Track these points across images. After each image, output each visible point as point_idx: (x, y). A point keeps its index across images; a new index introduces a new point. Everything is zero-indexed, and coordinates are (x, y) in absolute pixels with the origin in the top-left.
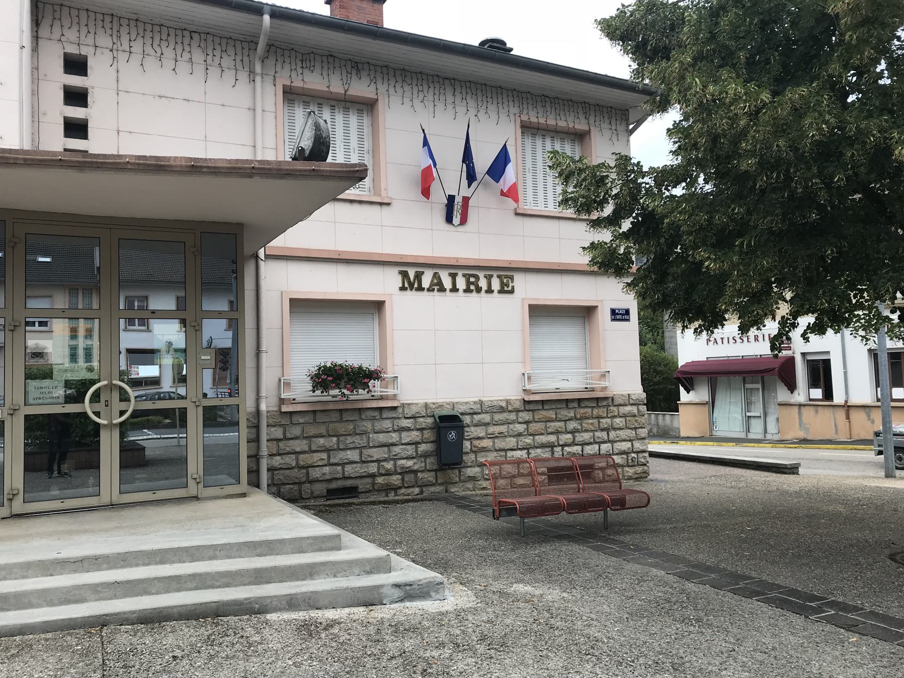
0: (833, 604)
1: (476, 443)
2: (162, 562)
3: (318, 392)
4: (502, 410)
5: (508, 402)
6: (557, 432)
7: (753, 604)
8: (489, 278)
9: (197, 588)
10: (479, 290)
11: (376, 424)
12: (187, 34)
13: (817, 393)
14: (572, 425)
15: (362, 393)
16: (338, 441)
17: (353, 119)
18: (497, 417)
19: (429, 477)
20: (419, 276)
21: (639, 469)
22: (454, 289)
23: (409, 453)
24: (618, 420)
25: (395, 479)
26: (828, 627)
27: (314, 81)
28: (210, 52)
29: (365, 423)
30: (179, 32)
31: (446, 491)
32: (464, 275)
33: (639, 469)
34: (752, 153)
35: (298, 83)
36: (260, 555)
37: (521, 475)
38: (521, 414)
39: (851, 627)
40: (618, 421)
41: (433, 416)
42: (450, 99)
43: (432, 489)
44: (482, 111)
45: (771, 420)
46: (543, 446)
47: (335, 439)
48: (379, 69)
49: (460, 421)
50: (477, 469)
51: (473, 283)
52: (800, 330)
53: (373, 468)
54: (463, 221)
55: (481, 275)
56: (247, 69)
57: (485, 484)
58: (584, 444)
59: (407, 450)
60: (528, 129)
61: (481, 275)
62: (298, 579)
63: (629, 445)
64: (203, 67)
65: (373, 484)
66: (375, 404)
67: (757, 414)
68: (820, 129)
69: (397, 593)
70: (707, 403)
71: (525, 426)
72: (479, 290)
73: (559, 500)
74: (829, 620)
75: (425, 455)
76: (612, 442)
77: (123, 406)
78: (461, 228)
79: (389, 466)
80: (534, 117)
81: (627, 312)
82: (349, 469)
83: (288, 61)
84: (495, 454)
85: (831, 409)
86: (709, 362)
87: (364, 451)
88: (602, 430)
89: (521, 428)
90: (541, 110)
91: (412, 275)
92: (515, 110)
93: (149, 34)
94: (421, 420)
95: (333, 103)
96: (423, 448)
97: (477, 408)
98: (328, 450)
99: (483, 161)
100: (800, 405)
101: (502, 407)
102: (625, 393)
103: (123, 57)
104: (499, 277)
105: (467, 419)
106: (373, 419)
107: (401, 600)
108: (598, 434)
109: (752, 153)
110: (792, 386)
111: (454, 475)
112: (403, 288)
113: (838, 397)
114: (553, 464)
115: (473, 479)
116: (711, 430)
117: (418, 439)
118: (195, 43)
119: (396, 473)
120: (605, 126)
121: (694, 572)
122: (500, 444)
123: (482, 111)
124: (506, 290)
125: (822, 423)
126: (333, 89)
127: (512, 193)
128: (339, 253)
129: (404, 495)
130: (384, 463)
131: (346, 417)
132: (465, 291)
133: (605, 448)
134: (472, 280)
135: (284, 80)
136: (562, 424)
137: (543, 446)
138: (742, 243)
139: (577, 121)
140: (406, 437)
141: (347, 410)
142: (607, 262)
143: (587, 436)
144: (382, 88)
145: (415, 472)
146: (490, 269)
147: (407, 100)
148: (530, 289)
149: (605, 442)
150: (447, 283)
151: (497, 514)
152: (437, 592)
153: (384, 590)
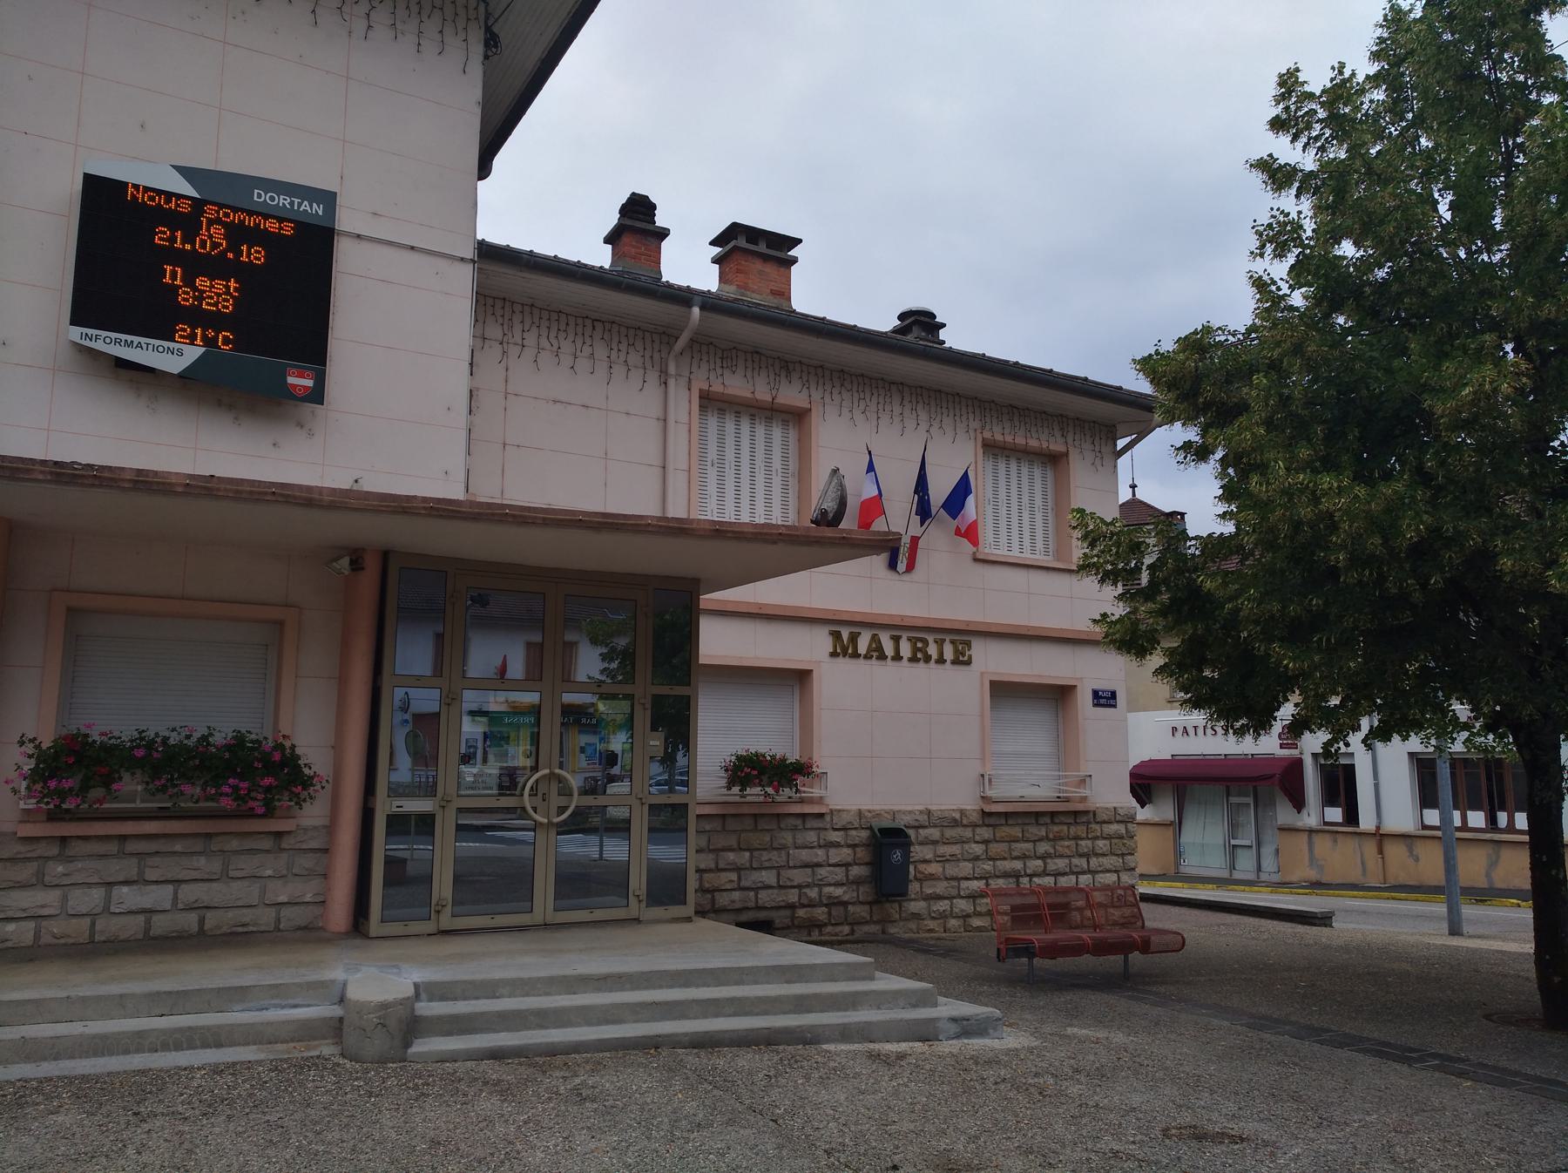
0: (1435, 1056)
1: (922, 867)
2: (687, 985)
3: (736, 790)
4: (955, 823)
5: (962, 812)
6: (1023, 857)
7: (1344, 1053)
8: (940, 643)
9: (735, 1015)
10: (927, 659)
11: (799, 835)
12: (588, 322)
13: (1335, 814)
14: (1043, 848)
15: (787, 792)
16: (752, 857)
17: (777, 433)
18: (949, 833)
19: (862, 911)
20: (854, 638)
21: (1127, 911)
22: (897, 657)
23: (838, 878)
24: (1101, 843)
25: (820, 913)
26: (1437, 1075)
27: (736, 384)
28: (614, 346)
29: (784, 834)
30: (580, 321)
31: (883, 932)
32: (909, 639)
33: (1127, 911)
34: (1343, 547)
35: (717, 388)
36: (788, 982)
37: (979, 914)
38: (978, 830)
39: (1462, 1074)
40: (1102, 844)
41: (871, 828)
42: (897, 410)
43: (866, 928)
44: (936, 425)
45: (1268, 851)
46: (1006, 875)
47: (747, 854)
48: (812, 370)
49: (907, 836)
50: (923, 904)
51: (920, 650)
52: (1361, 735)
53: (793, 896)
54: (910, 567)
55: (931, 639)
56: (657, 367)
57: (932, 924)
58: (1058, 874)
59: (835, 872)
60: (992, 449)
61: (931, 639)
62: (839, 1010)
63: (1114, 877)
64: (605, 365)
65: (793, 918)
66: (797, 809)
67: (1247, 843)
68: (1418, 529)
69: (954, 1028)
70: (1171, 824)
71: (983, 847)
72: (927, 659)
73: (1065, 938)
74: (1436, 1068)
75: (857, 882)
76: (1094, 872)
77: (562, 801)
78: (906, 577)
79: (813, 893)
80: (1000, 433)
81: (1113, 695)
82: (764, 896)
83: (705, 358)
84: (945, 883)
85: (1357, 839)
86: (1175, 761)
87: (783, 872)
88: (1081, 856)
89: (978, 849)
90: (1007, 425)
91: (845, 636)
92: (975, 424)
93: (545, 323)
94: (854, 833)
95: (753, 411)
96: (856, 871)
97: (923, 819)
98: (738, 869)
99: (939, 491)
100: (1311, 831)
101: (955, 820)
102: (1110, 806)
103: (514, 351)
104: (952, 642)
105: (911, 832)
106: (795, 829)
107: (958, 1037)
108: (1075, 861)
109: (1343, 547)
110: (1299, 803)
111: (892, 909)
112: (834, 654)
113: (1367, 822)
114: (1018, 901)
115: (916, 916)
116: (1177, 864)
117: (850, 859)
118: (598, 333)
119: (821, 904)
120: (1087, 446)
121: (1261, 1023)
122: (951, 870)
123: (936, 425)
124: (961, 660)
125: (1341, 858)
126: (759, 396)
127: (970, 533)
128: (761, 606)
129: (830, 934)
130: (807, 890)
131: (762, 825)
132: (910, 660)
133: (1085, 880)
134: (919, 645)
135: (699, 384)
136: (1029, 846)
137: (1006, 875)
138: (1320, 639)
139: (1052, 439)
140: (836, 856)
141: (763, 815)
142: (1129, 639)
143: (1061, 864)
144: (817, 395)
145: (845, 904)
146: (942, 631)
147: (845, 411)
148: (993, 661)
149: (1084, 873)
150: (889, 649)
151: (1003, 954)
152: (995, 1029)
153: (940, 1024)
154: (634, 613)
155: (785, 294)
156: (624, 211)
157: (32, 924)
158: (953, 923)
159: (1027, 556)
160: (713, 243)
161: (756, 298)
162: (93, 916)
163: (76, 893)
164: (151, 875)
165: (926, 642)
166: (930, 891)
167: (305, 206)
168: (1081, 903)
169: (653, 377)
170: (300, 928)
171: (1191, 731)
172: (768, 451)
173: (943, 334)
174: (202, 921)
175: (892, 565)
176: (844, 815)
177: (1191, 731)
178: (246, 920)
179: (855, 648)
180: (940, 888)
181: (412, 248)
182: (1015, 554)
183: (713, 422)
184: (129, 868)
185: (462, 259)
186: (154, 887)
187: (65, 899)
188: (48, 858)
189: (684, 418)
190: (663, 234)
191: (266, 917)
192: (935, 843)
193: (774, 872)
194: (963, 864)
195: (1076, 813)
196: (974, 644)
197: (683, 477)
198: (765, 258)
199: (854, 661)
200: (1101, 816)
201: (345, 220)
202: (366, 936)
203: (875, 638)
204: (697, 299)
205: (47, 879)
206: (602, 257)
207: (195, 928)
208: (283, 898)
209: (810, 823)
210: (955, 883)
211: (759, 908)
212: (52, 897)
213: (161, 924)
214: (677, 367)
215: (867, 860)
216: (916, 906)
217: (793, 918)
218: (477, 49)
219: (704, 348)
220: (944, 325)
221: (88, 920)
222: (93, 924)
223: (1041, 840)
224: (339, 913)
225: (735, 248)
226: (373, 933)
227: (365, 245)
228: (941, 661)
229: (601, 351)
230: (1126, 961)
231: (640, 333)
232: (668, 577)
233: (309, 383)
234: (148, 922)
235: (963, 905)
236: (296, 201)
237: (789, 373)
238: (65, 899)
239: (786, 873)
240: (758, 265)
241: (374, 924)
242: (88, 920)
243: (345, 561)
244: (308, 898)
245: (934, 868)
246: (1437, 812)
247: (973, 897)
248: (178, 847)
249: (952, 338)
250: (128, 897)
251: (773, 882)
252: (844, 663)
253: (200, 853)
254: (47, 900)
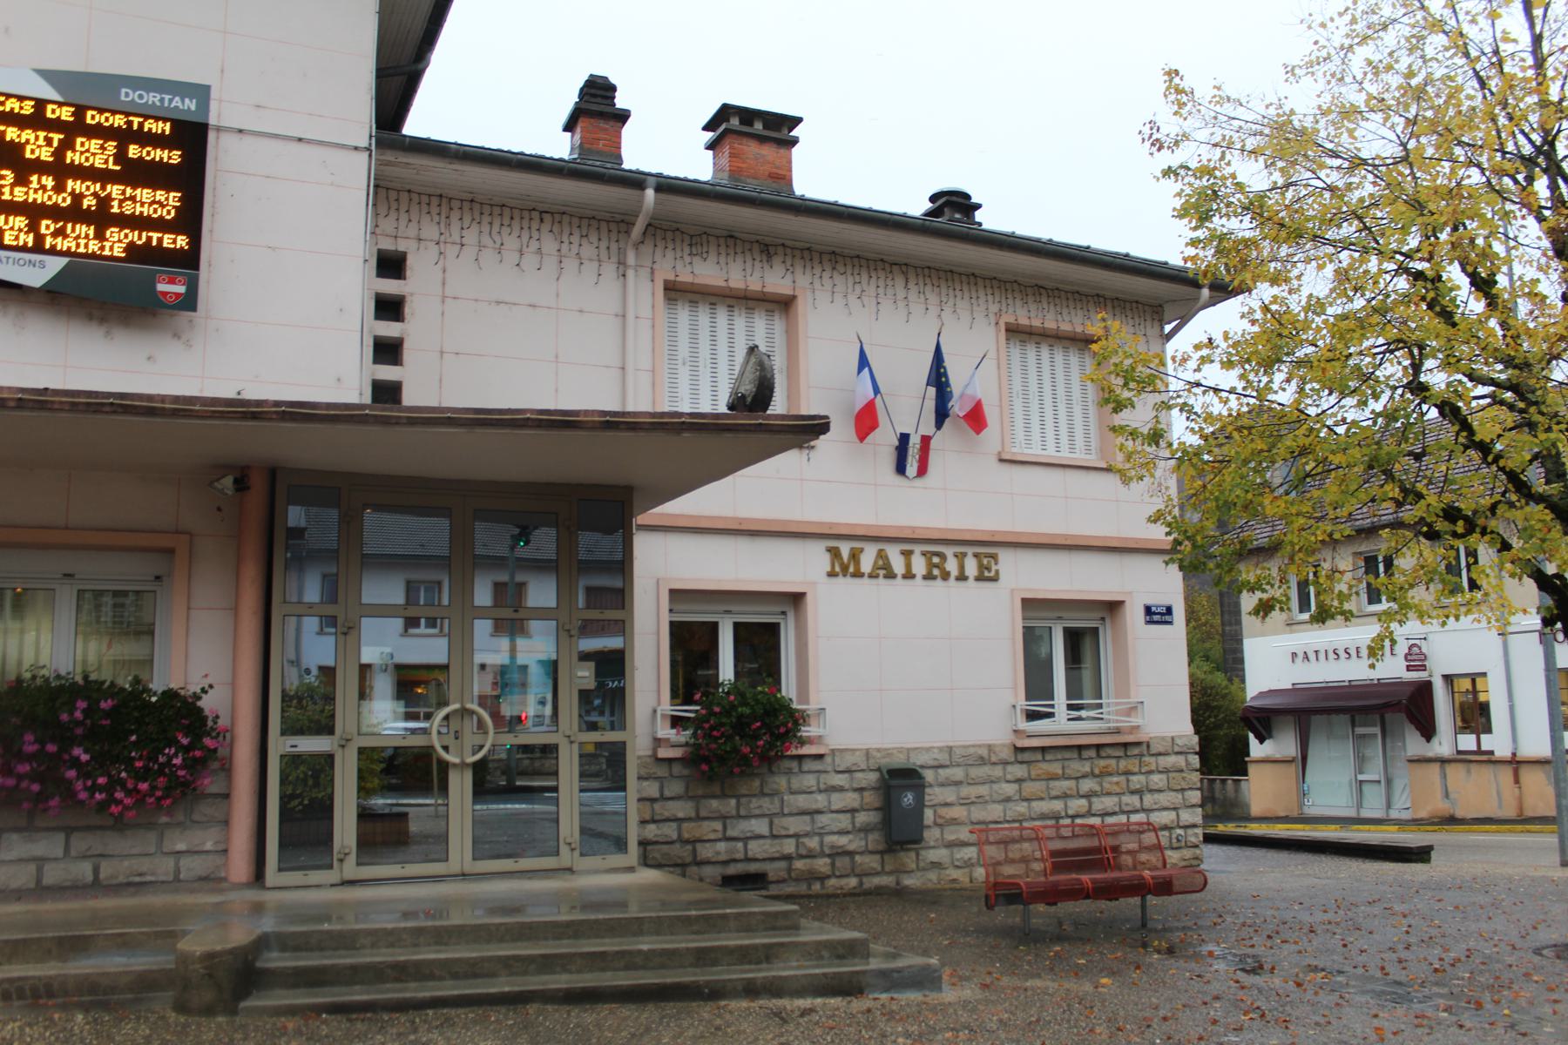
1: (943, 811)
4: (982, 761)
5: (990, 747)
8: (960, 557)
10: (946, 576)
12: (536, 215)
14: (1087, 785)
18: (977, 772)
19: (872, 862)
20: (855, 556)
21: (1188, 853)
24: (1155, 778)
25: (822, 865)
27: (708, 271)
28: (565, 238)
30: (526, 214)
35: (685, 277)
37: (1013, 861)
38: (1009, 768)
40: (1158, 780)
42: (901, 293)
44: (948, 310)
48: (798, 253)
49: (920, 777)
51: (936, 566)
53: (789, 847)
54: (922, 471)
56: (614, 259)
61: (949, 551)
63: (1173, 815)
64: (555, 260)
65: (789, 870)
67: (1375, 777)
71: (1015, 786)
72: (946, 576)
75: (865, 830)
76: (1148, 811)
78: (919, 482)
79: (813, 843)
81: (1169, 610)
82: (755, 848)
83: (671, 246)
85: (1491, 767)
87: (776, 821)
88: (1132, 793)
89: (1010, 789)
91: (845, 554)
93: (486, 219)
95: (731, 301)
96: (862, 818)
97: (943, 758)
98: (724, 818)
100: (1443, 761)
101: (982, 758)
104: (976, 555)
108: (1126, 799)
111: (909, 859)
112: (832, 574)
114: (1058, 845)
115: (936, 865)
116: (1301, 805)
117: (856, 805)
119: (823, 854)
124: (986, 576)
126: (733, 284)
128: (741, 520)
130: (805, 840)
132: (925, 578)
134: (936, 560)
136: (1072, 783)
137: (1043, 817)
140: (838, 800)
145: (851, 854)
147: (838, 298)
149: (1136, 811)
150: (898, 565)
159: (1065, 455)
160: (706, 128)
166: (952, 837)
167: (177, 102)
169: (610, 269)
171: (1312, 656)
173: (979, 216)
174: (96, 871)
175: (901, 469)
177: (1312, 656)
181: (300, 140)
182: (1050, 454)
183: (683, 314)
185: (356, 148)
189: (646, 312)
190: (623, 117)
192: (958, 783)
193: (766, 820)
194: (991, 807)
195: (1125, 745)
196: (1001, 557)
197: (645, 379)
199: (857, 581)
201: (216, 116)
203: (881, 554)
204: (652, 180)
206: (560, 146)
211: (748, 860)
214: (637, 256)
215: (877, 805)
216: (933, 855)
217: (789, 870)
219: (669, 234)
220: (978, 206)
223: (1084, 776)
225: (726, 131)
227: (248, 139)
228: (962, 577)
229: (550, 245)
230: (1143, 906)
231: (594, 223)
232: (548, 484)
233: (181, 289)
236: (167, 97)
237: (769, 257)
243: (228, 481)
245: (958, 812)
246: (553, 604)
249: (988, 219)
251: (765, 830)
252: (842, 582)
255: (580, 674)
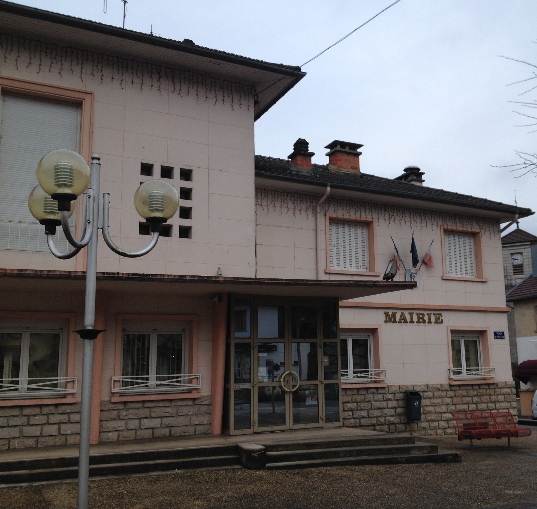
1: (426, 408)
4: (439, 390)
5: (441, 385)
6: (468, 403)
10: (424, 322)
14: (476, 399)
18: (437, 394)
19: (401, 427)
20: (394, 315)
22: (412, 322)
24: (500, 397)
38: (448, 392)
40: (501, 398)
47: (355, 404)
49: (420, 395)
57: (431, 432)
61: (425, 313)
71: (451, 399)
72: (424, 322)
75: (400, 415)
80: (450, 226)
84: (436, 415)
87: (370, 411)
88: (492, 402)
89: (448, 400)
94: (397, 395)
96: (399, 410)
97: (425, 388)
98: (352, 410)
101: (439, 389)
102: (504, 381)
105: (421, 394)
106: (374, 393)
108: (490, 405)
111: (415, 426)
112: (386, 322)
114: (466, 422)
115: (424, 428)
117: (396, 406)
119: (386, 424)
122: (438, 409)
124: (439, 321)
132: (417, 323)
136: (470, 399)
144: (375, 216)
145: (395, 424)
150: (408, 318)
154: (309, 311)
155: (357, 168)
156: (296, 146)
157: (116, 433)
158: (439, 431)
160: (327, 147)
161: (346, 171)
162: (136, 430)
163: (130, 422)
164: (153, 415)
165: (423, 315)
168: (493, 423)
169: (310, 212)
170: (202, 434)
172: (356, 239)
174: (170, 431)
176: (393, 388)
178: (185, 431)
179: (395, 318)
180: (433, 417)
182: (459, 276)
183: (334, 228)
184: (146, 412)
186: (154, 419)
187: (127, 424)
188: (121, 409)
191: (191, 430)
192: (430, 398)
195: (489, 385)
198: (348, 154)
199: (394, 324)
200: (499, 386)
202: (229, 435)
203: (402, 315)
205: (120, 417)
207: (168, 434)
208: (197, 423)
209: (380, 391)
210: (440, 415)
212: (122, 423)
213: (158, 433)
215: (403, 406)
216: (425, 424)
218: (252, 104)
220: (424, 173)
221: (134, 432)
222: (136, 433)
223: (474, 396)
224: (217, 428)
226: (231, 434)
228: (430, 322)
229: (291, 205)
234: (153, 432)
235: (443, 424)
238: (127, 424)
239: (371, 412)
240: (346, 157)
241: (232, 431)
242: (134, 432)
244: (205, 422)
245: (431, 409)
247: (447, 420)
248: (161, 405)
250: (147, 423)
253: (168, 407)
254: (120, 424)
255: (325, 360)
